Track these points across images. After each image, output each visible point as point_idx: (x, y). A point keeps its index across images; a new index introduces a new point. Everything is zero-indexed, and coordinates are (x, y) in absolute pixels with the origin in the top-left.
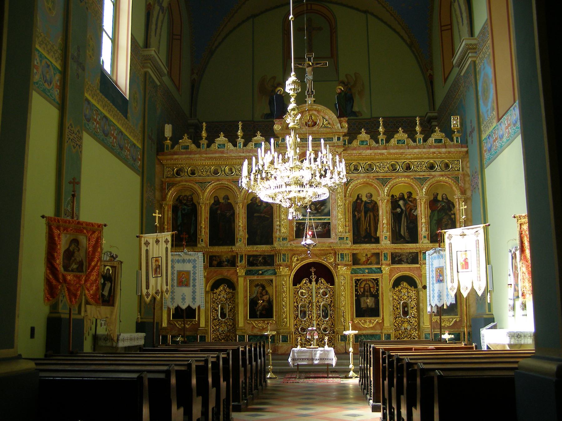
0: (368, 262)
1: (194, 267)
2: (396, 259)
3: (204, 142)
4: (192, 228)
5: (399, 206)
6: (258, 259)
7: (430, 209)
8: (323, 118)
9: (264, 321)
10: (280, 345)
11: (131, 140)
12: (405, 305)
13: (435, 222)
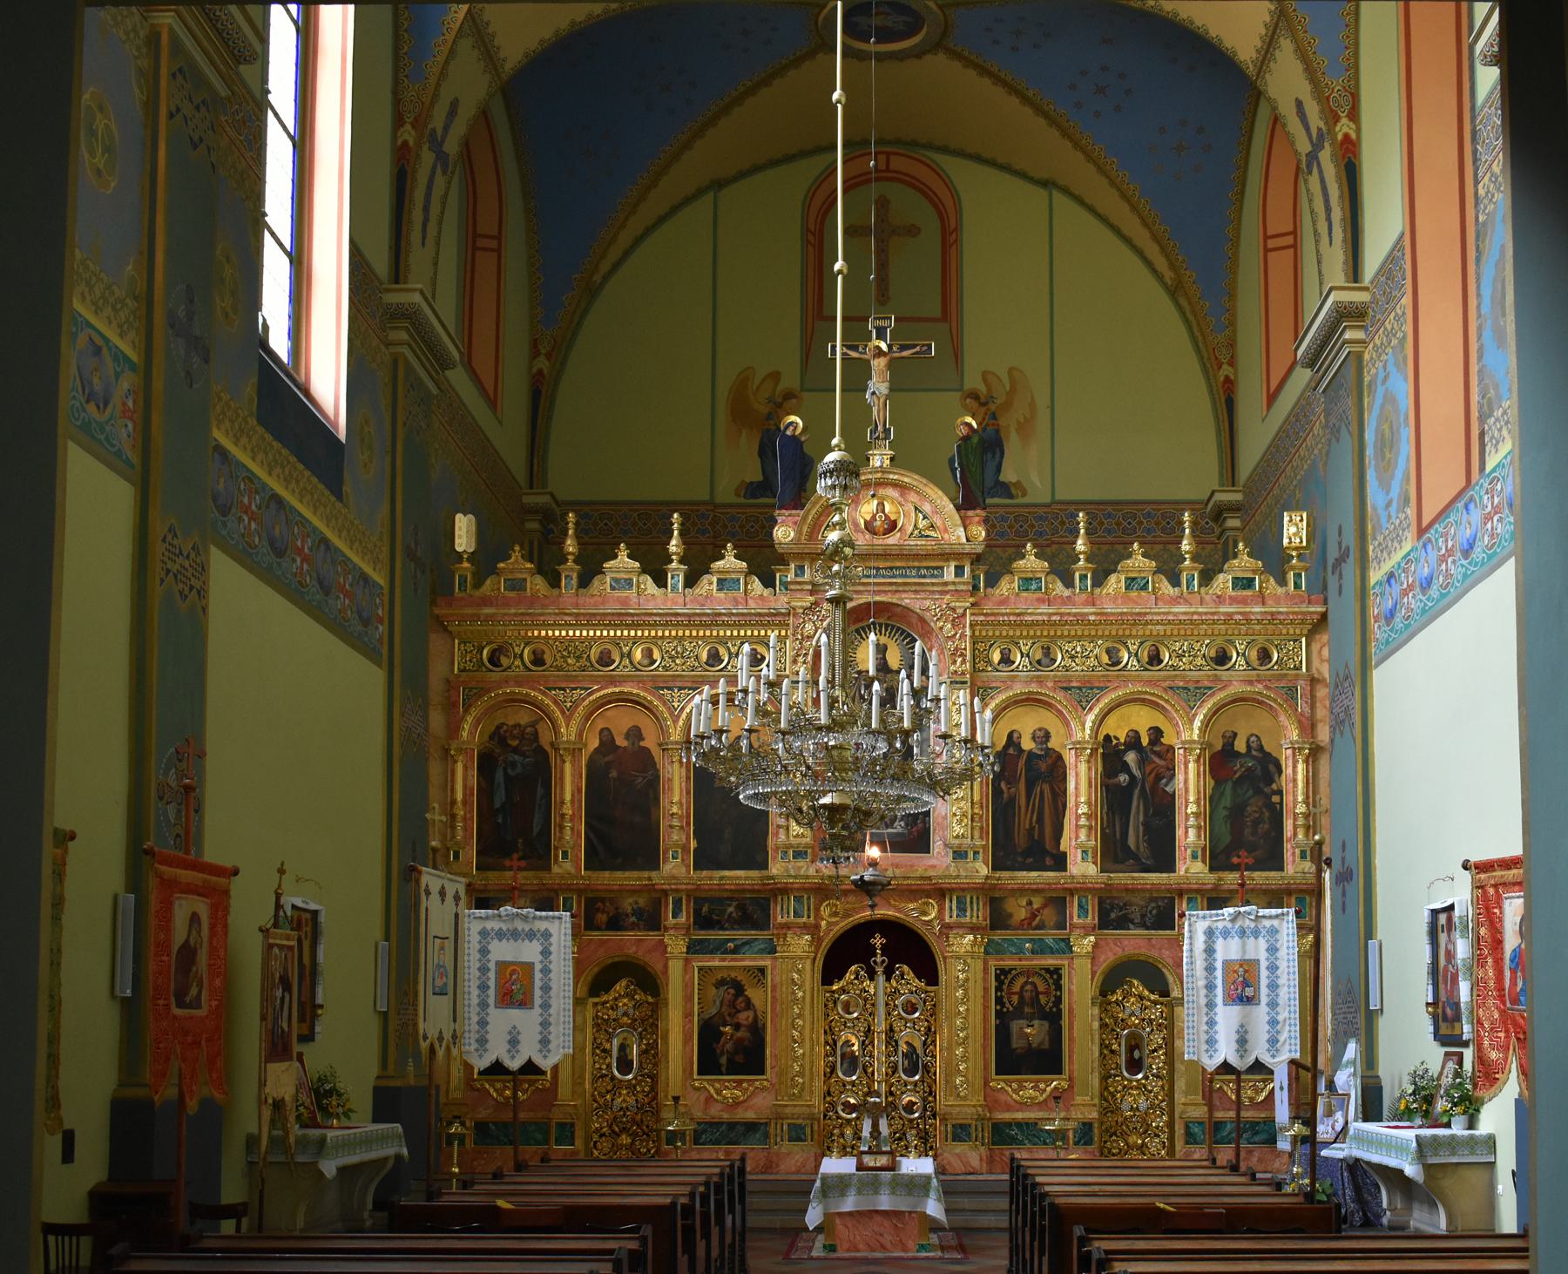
0: (1034, 924)
1: (546, 953)
2: (1113, 916)
3: (570, 570)
4: (536, 820)
5: (1126, 768)
6: (725, 911)
7: (1213, 778)
8: (916, 508)
9: (740, 1082)
10: (783, 1150)
11: (355, 565)
12: (1135, 1044)
13: (1225, 813)
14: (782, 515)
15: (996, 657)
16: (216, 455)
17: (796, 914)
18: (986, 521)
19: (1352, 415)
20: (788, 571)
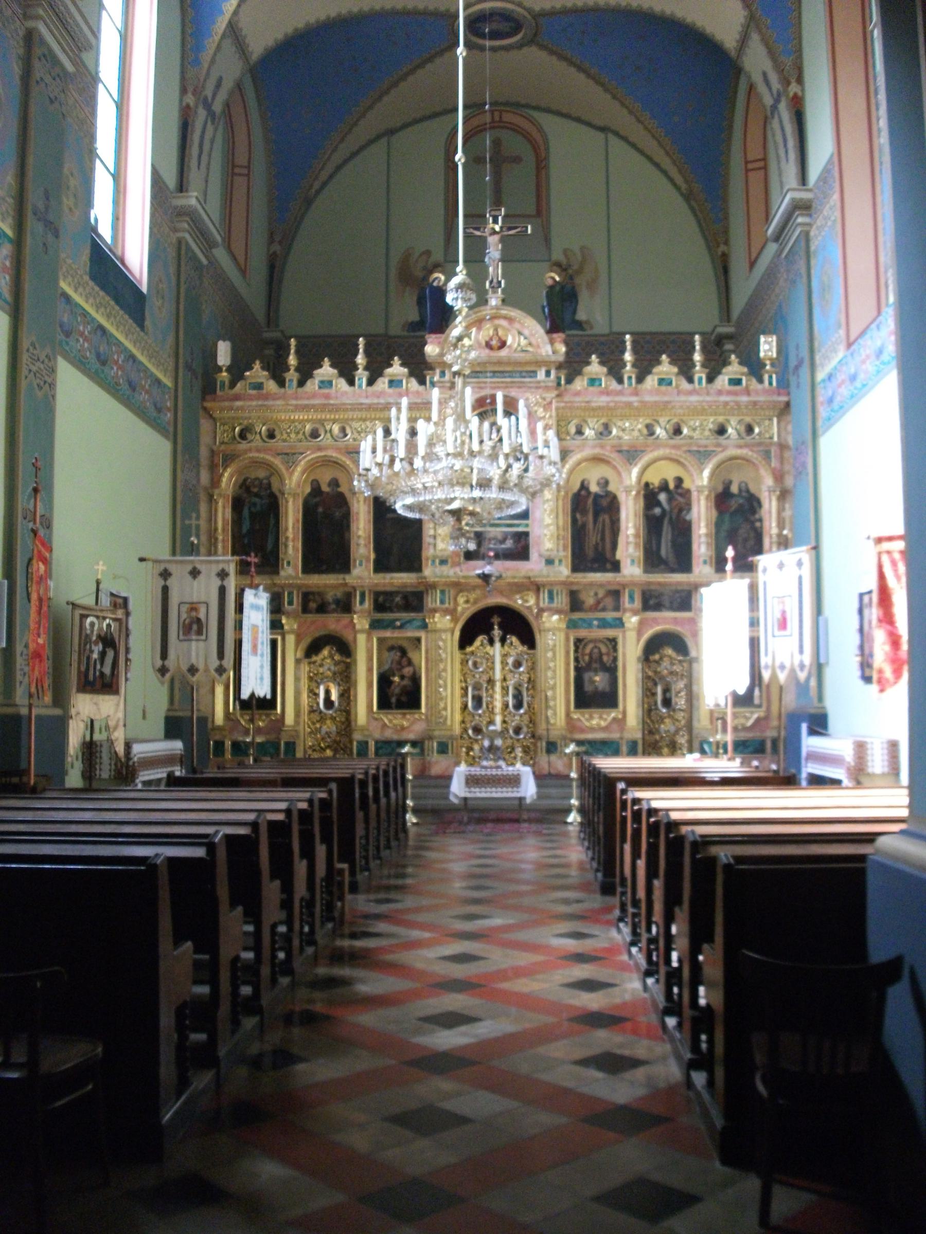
3: (292, 376)
5: (659, 504)
14: (431, 338)
15: (573, 430)
16: (63, 299)
17: (442, 602)
18: (567, 344)
19: (803, 271)
20: (434, 374)
